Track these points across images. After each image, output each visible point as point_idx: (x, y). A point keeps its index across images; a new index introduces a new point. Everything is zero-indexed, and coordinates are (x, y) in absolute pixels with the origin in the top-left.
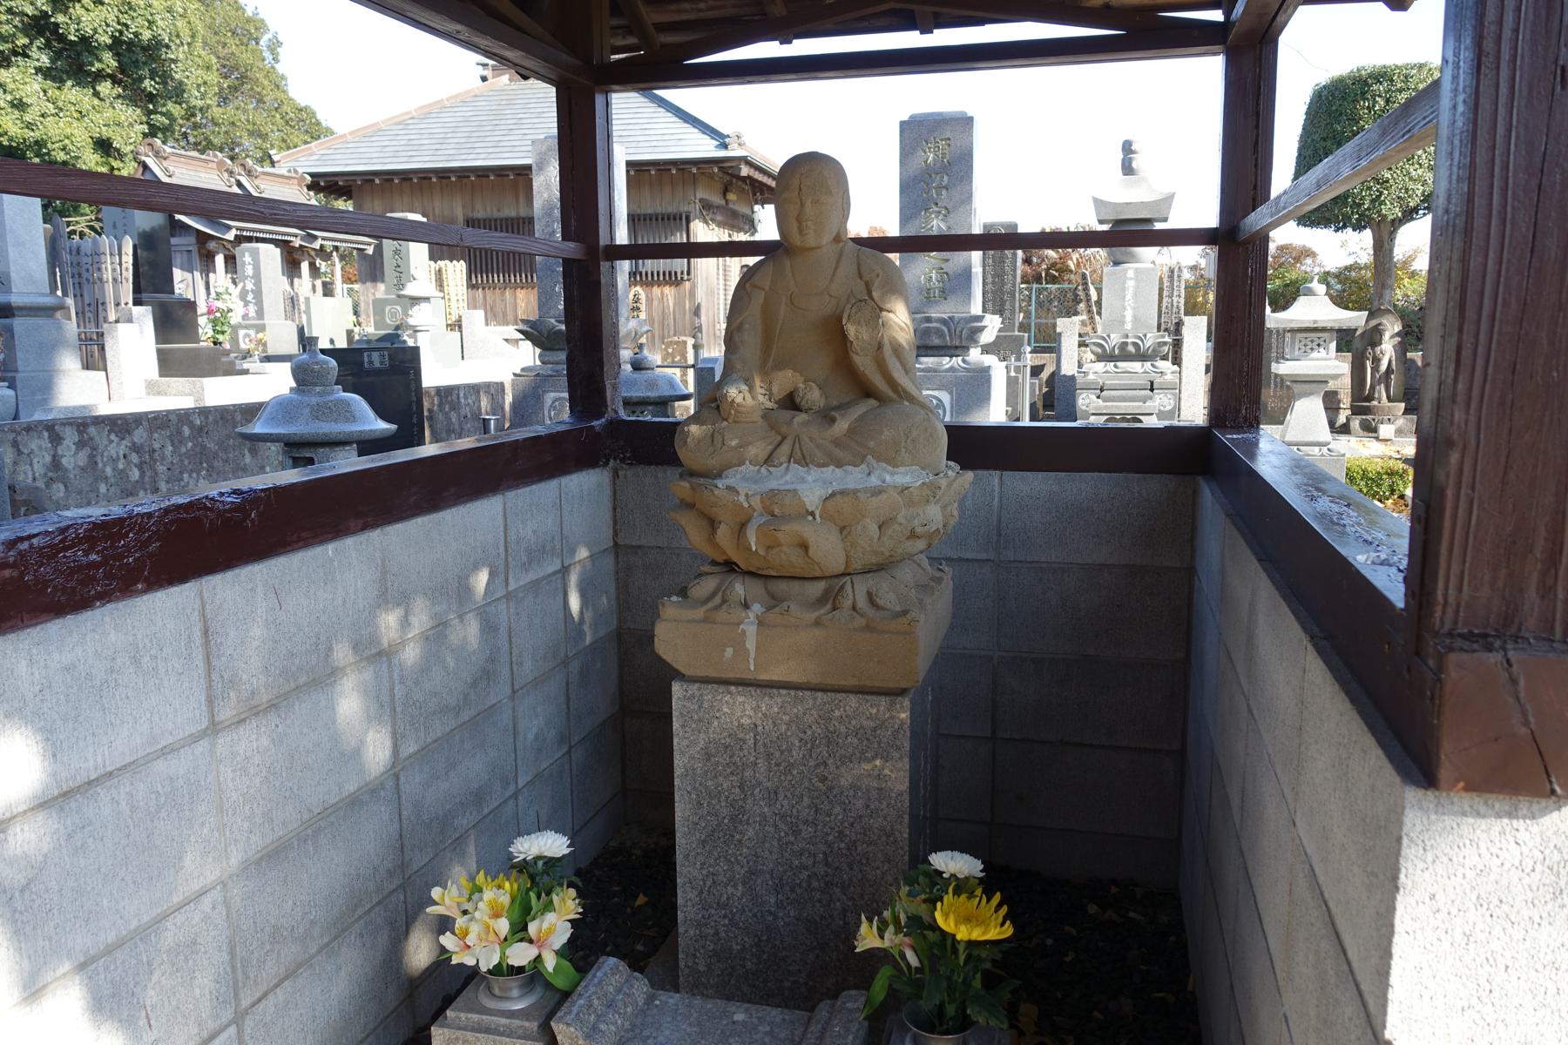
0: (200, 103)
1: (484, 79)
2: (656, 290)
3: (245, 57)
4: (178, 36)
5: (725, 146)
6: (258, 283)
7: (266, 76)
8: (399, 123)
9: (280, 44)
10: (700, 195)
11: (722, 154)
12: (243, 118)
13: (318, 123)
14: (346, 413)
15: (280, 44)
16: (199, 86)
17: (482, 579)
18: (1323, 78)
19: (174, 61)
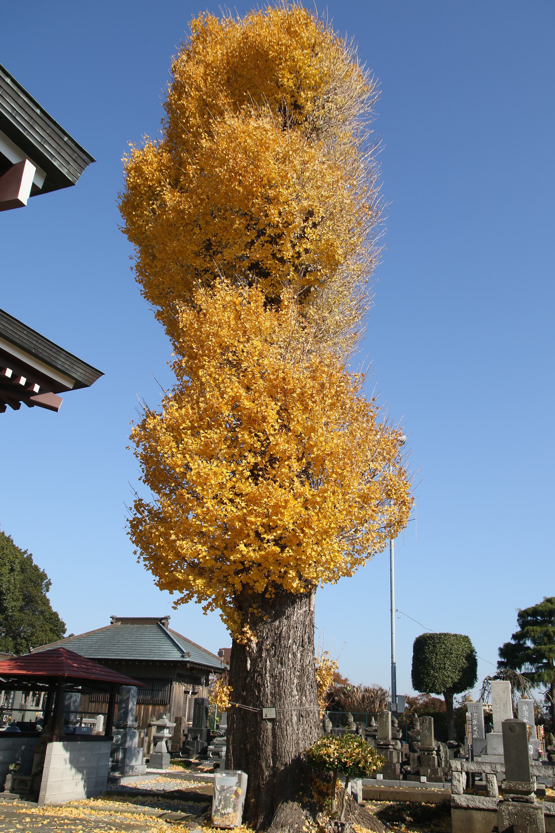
0: (11, 614)
1: (112, 623)
2: (157, 707)
3: (34, 593)
4: (9, 590)
5: (183, 656)
6: (13, 701)
7: (41, 600)
8: (77, 639)
9: (51, 584)
10: (176, 672)
11: (182, 659)
12: (27, 618)
13: (59, 620)
14: (16, 729)
15: (51, 584)
16: (12, 607)
17: (23, 747)
18: (418, 636)
19: (5, 599)
